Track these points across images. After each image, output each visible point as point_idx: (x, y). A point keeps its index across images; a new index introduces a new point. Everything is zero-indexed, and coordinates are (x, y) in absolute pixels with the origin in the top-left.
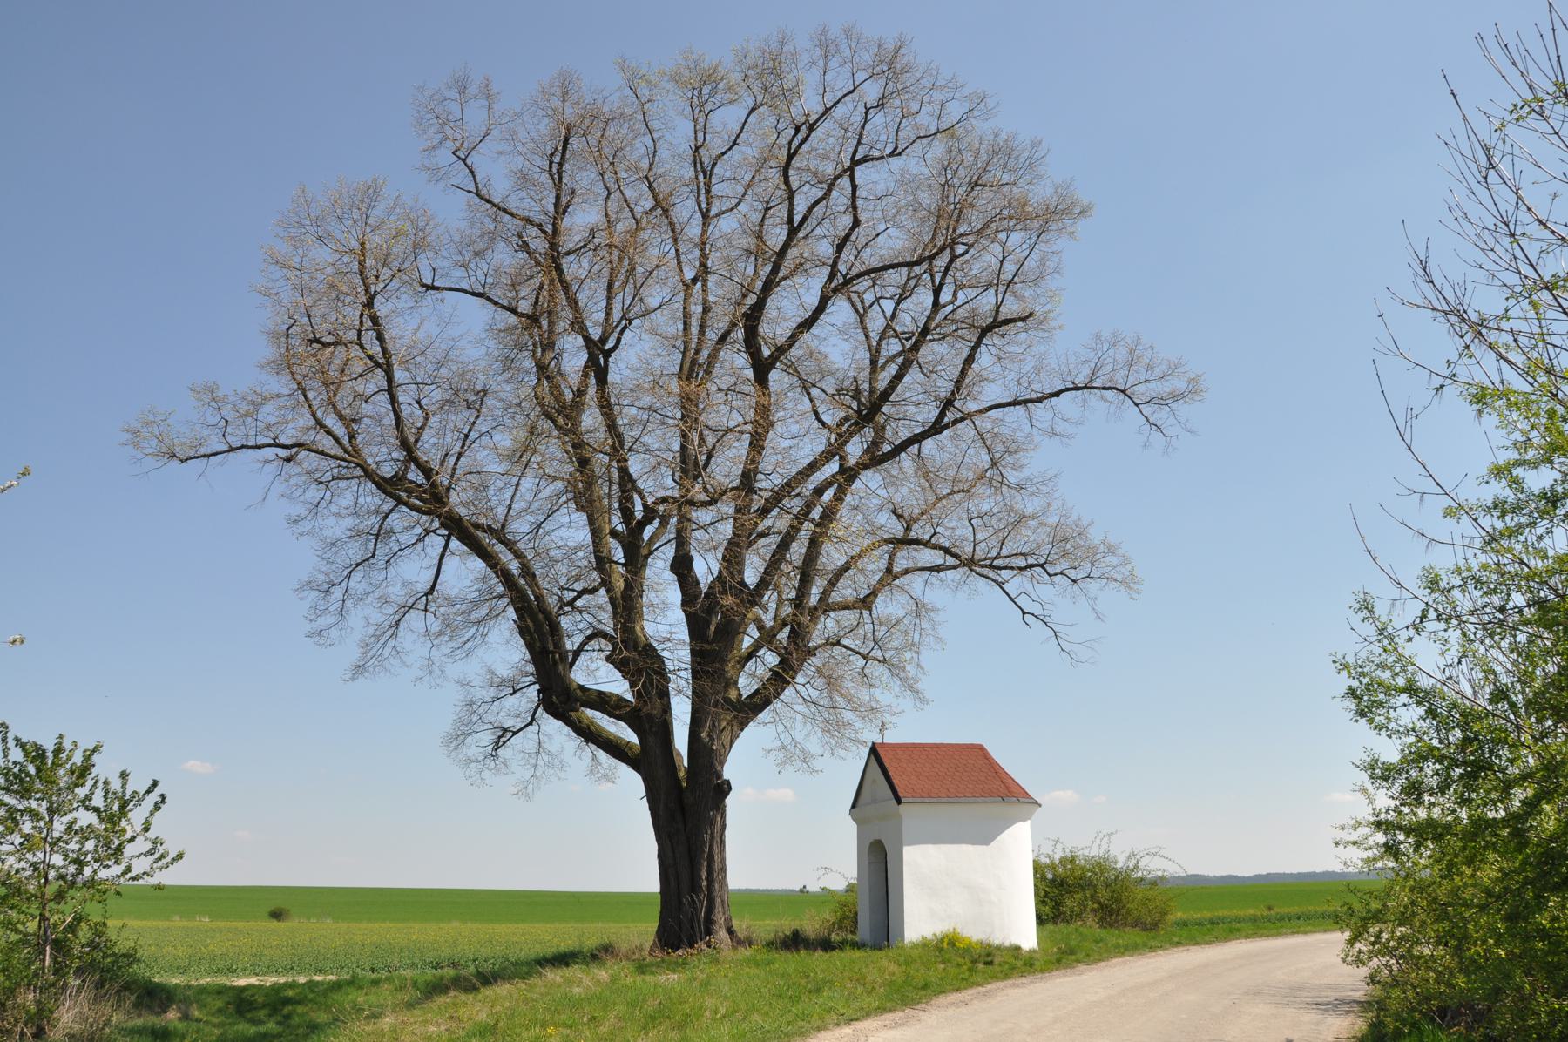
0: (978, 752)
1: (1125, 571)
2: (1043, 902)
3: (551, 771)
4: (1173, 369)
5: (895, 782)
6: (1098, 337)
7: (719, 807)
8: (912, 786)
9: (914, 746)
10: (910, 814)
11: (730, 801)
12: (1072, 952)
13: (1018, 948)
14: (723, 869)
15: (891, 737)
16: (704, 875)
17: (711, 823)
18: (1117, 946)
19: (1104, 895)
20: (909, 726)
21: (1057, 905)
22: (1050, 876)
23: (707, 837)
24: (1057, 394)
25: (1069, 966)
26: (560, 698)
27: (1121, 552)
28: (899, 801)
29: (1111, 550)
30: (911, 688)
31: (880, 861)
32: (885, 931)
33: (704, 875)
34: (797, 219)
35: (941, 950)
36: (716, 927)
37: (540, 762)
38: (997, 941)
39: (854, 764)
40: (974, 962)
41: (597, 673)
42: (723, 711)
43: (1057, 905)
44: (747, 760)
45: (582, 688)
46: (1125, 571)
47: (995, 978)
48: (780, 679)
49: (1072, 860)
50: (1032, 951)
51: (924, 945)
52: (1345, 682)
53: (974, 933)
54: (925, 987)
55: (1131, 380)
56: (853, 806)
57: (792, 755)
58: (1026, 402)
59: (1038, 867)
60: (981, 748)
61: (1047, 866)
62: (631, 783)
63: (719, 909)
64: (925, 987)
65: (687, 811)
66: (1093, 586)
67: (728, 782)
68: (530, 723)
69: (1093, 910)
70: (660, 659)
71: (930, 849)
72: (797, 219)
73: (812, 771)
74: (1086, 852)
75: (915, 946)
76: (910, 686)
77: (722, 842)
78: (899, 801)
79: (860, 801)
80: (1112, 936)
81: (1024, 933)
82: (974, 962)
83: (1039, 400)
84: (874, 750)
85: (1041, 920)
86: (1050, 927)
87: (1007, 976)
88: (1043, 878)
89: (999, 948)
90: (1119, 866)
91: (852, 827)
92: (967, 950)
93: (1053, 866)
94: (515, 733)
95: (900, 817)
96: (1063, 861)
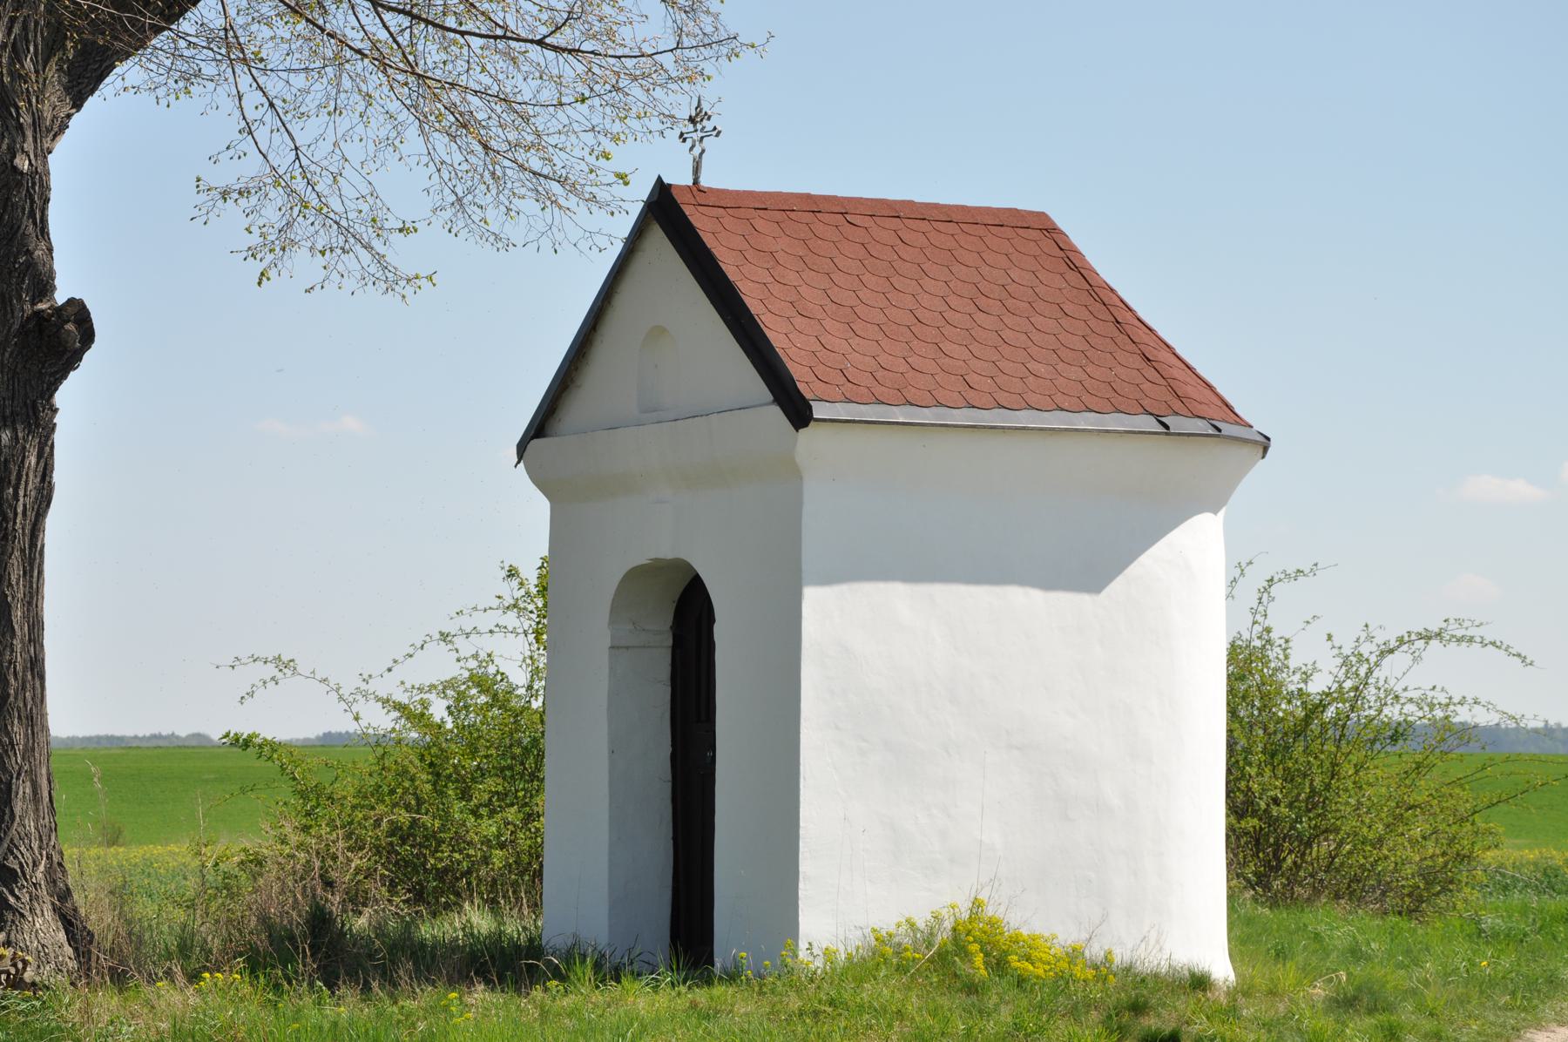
5: (777, 338)
28: (798, 413)
31: (687, 661)
51: (883, 960)
56: (541, 426)
57: (300, 215)
60: (1044, 228)
67: (78, 313)
71: (899, 600)
73: (390, 279)
78: (798, 413)
79: (576, 410)
84: (664, 208)
95: (794, 474)
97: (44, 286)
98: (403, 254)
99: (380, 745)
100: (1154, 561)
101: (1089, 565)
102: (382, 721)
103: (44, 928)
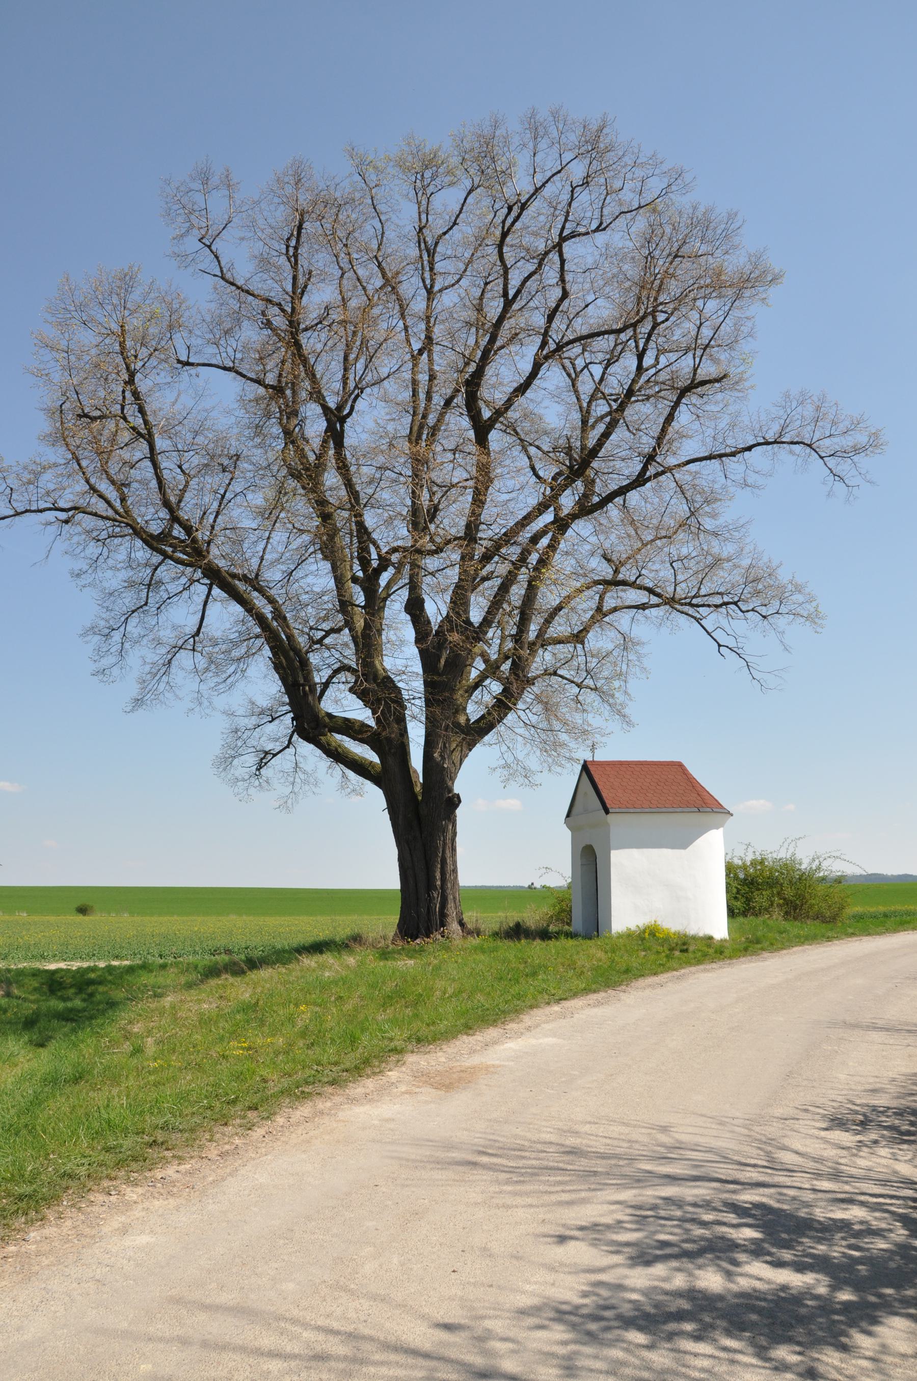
2: (736, 898)
3: (307, 787)
4: (856, 425)
5: (604, 795)
8: (623, 798)
9: (621, 763)
12: (758, 942)
13: (711, 938)
14: (455, 871)
17: (444, 830)
19: (789, 893)
21: (748, 900)
22: (742, 876)
23: (440, 843)
24: (749, 449)
25: (755, 953)
26: (312, 725)
27: (807, 590)
28: (607, 811)
31: (591, 863)
34: (511, 293)
35: (643, 939)
36: (449, 920)
37: (298, 780)
39: (570, 777)
41: (343, 703)
42: (455, 733)
46: (810, 607)
47: (689, 963)
49: (762, 862)
51: (629, 935)
53: (673, 925)
54: (627, 971)
56: (568, 816)
57: (515, 772)
58: (721, 456)
59: (730, 869)
60: (680, 765)
61: (739, 867)
62: (375, 796)
63: (451, 904)
64: (627, 971)
65: (423, 819)
66: (781, 622)
68: (288, 747)
69: (779, 905)
71: (635, 853)
72: (511, 293)
73: (533, 785)
74: (775, 856)
75: (620, 936)
77: (454, 849)
78: (607, 811)
79: (574, 812)
80: (794, 928)
81: (716, 924)
82: (672, 949)
83: (733, 454)
84: (585, 768)
85: (732, 913)
86: (741, 919)
87: (699, 962)
88: (736, 878)
89: (694, 938)
90: (803, 867)
93: (744, 867)
94: (275, 755)
95: (607, 825)
96: (754, 863)
98: (537, 778)
101: (683, 842)
103: (455, 926)
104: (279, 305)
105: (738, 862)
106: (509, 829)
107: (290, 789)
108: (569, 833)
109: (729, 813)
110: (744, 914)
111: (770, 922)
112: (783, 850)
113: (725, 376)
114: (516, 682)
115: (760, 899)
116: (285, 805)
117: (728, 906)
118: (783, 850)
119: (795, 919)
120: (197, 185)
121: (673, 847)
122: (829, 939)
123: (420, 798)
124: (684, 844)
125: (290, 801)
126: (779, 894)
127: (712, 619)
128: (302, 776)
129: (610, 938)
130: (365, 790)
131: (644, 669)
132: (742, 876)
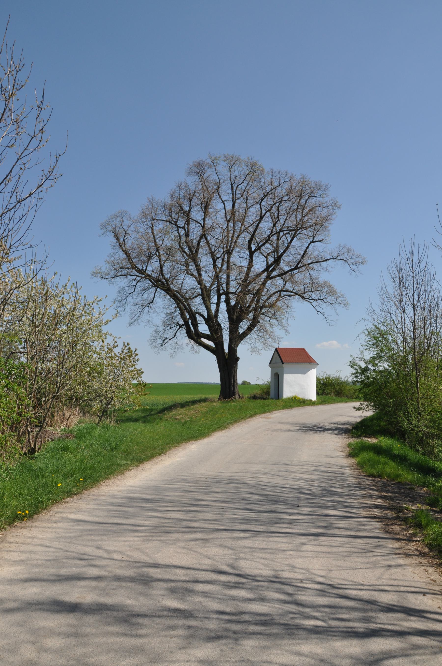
0: (303, 350)
1: (345, 302)
2: (320, 389)
3: (179, 350)
4: (358, 256)
5: (282, 358)
6: (340, 246)
7: (236, 364)
8: (288, 359)
9: (287, 349)
10: (286, 367)
11: (239, 363)
12: (325, 402)
13: (311, 400)
14: (237, 379)
15: (281, 347)
16: (232, 381)
17: (235, 368)
18: (337, 401)
19: (337, 388)
20: (287, 343)
21: (324, 390)
22: (322, 382)
23: (233, 371)
24: (328, 260)
25: (323, 404)
26: (195, 336)
27: (344, 296)
28: (283, 363)
29: (342, 296)
30: (285, 329)
31: (277, 378)
32: (278, 394)
33: (232, 381)
34: (263, 215)
35: (293, 400)
36: (236, 394)
37: (176, 348)
38: (306, 398)
39: (271, 352)
40: (301, 402)
41: (204, 328)
42: (236, 338)
43: (324, 390)
44: (242, 349)
45: (202, 333)
46: (345, 302)
47: (306, 405)
48: (250, 329)
49: (329, 378)
50: (315, 401)
51: (288, 399)
52: (351, 359)
53: (301, 396)
54: (291, 406)
55: (348, 258)
56: (270, 363)
57: (254, 350)
58: (320, 262)
59: (318, 380)
60: (304, 349)
61: (321, 379)
62: (213, 358)
63: (236, 389)
64: (291, 406)
65: (228, 364)
66: (336, 306)
67: (239, 357)
68: (174, 337)
69: (334, 392)
70: (221, 327)
71: (290, 375)
72: (263, 215)
73: (260, 354)
74: (333, 376)
75: (286, 399)
76: (283, 327)
77: (236, 373)
78: (283, 363)
79: (272, 362)
80: (339, 399)
81: (313, 397)
82: (301, 402)
83: (323, 261)
84: (276, 350)
85: (318, 394)
86: (321, 396)
87: (308, 405)
88: (320, 382)
89: (307, 400)
90: (342, 380)
91: (269, 369)
92: (299, 400)
93: (323, 379)
94: (170, 340)
95: (283, 367)
96: (326, 378)
97: (237, 356)
98: (261, 352)
99: (266, 384)
100: (309, 372)
101: (304, 373)
102: (266, 383)
103: (237, 396)
104: (200, 223)
105: (321, 378)
106: (253, 368)
107: (174, 350)
108: (270, 369)
109: (318, 364)
110: (322, 394)
111: (330, 397)
112: (336, 374)
113: (322, 240)
114: (254, 323)
115: (328, 390)
116: (172, 356)
117: (317, 392)
118: (336, 374)
119: (339, 396)
120: (178, 189)
121: (301, 374)
122: (346, 402)
123: (227, 357)
124: (305, 373)
125: (174, 355)
126: (334, 388)
127: (314, 303)
128: (178, 346)
129: (283, 400)
130: (201, 351)
131: (293, 317)
132: (322, 382)
